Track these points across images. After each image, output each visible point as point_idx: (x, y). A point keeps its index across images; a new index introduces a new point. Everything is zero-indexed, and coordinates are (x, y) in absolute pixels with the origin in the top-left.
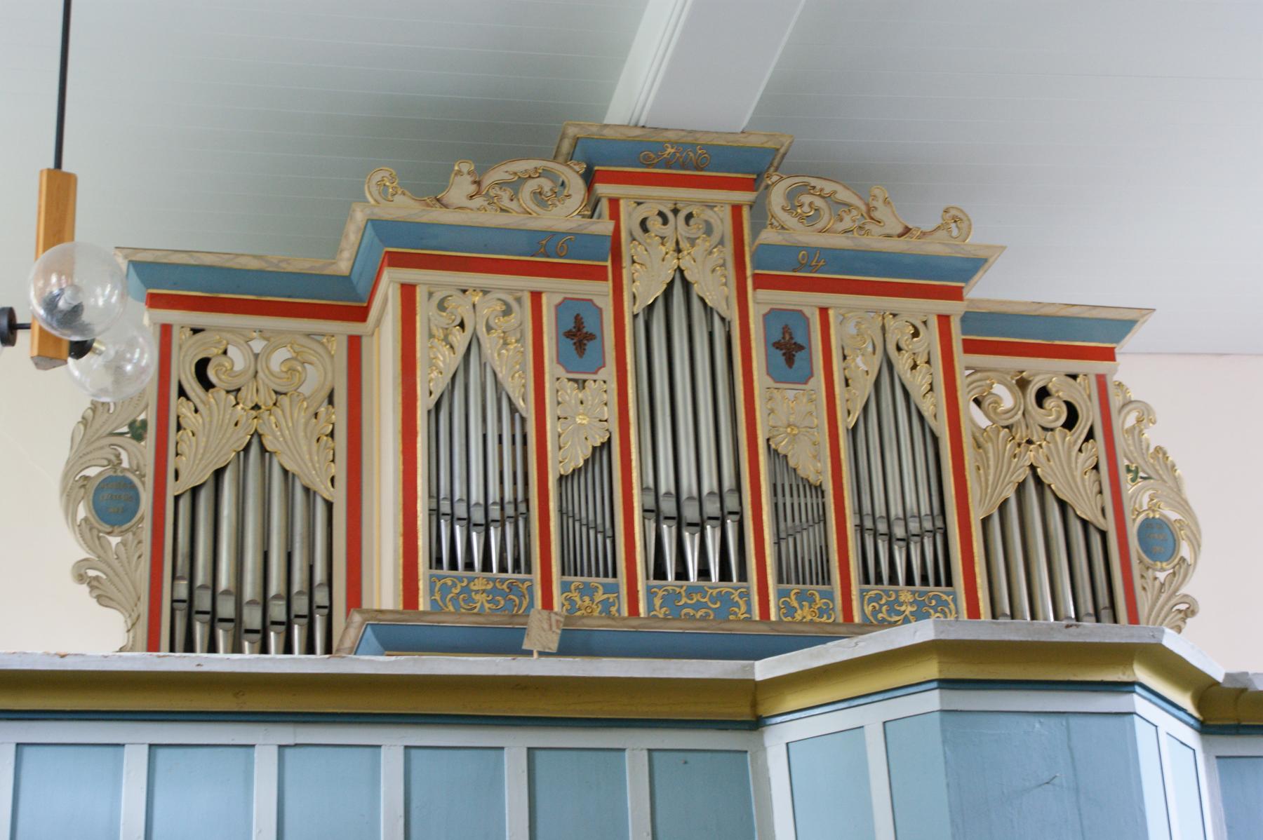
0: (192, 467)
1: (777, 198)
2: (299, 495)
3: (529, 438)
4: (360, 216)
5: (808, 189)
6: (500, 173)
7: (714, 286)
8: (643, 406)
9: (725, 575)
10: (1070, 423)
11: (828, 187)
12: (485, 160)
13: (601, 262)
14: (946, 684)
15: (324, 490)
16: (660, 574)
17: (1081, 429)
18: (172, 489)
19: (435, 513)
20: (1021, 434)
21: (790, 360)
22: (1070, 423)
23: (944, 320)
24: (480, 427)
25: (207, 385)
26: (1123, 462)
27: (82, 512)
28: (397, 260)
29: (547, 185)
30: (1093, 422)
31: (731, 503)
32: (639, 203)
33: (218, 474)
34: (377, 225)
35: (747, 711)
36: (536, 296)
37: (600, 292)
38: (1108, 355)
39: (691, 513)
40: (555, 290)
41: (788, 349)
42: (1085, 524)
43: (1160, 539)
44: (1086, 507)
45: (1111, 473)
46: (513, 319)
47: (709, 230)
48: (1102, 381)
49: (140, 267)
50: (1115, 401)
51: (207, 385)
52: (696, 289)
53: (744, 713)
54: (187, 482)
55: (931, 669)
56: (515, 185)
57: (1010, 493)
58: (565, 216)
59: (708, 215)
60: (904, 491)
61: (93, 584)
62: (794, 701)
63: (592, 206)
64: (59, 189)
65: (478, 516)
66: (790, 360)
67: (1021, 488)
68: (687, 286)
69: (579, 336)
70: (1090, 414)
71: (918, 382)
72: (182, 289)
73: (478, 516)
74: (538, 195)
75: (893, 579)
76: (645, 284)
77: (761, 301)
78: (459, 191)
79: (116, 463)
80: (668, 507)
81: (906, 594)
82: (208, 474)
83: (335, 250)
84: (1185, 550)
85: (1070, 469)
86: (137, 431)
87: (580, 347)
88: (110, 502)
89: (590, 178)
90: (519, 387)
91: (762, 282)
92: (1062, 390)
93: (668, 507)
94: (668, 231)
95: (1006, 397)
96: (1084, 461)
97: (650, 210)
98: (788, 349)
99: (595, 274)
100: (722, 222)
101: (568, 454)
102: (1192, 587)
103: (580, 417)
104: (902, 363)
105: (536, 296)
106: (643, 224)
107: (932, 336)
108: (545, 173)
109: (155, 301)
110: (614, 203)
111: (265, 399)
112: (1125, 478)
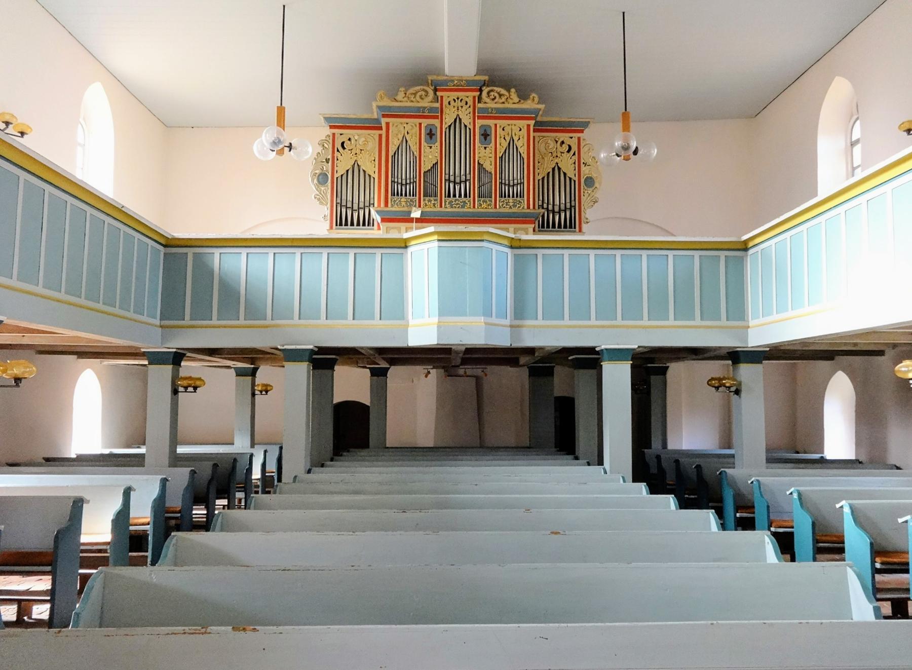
0: (341, 171)
1: (484, 94)
2: (367, 176)
3: (418, 160)
4: (374, 105)
5: (492, 91)
6: (412, 90)
7: (467, 120)
8: (446, 152)
9: (465, 196)
10: (569, 151)
11: (499, 89)
12: (408, 86)
13: (438, 113)
14: (439, 240)
15: (372, 175)
16: (449, 196)
17: (572, 152)
18: (336, 176)
19: (393, 182)
20: (554, 155)
21: (485, 139)
22: (569, 151)
23: (529, 126)
24: (403, 160)
25: (344, 148)
26: (582, 161)
27: (315, 181)
28: (384, 116)
29: (423, 93)
30: (575, 151)
31: (468, 178)
32: (448, 96)
33: (347, 171)
34: (379, 107)
35: (404, 245)
36: (420, 124)
37: (437, 122)
38: (582, 131)
39: (458, 180)
40: (425, 122)
41: (485, 135)
42: (570, 179)
43: (590, 182)
44: (570, 174)
45: (579, 164)
46: (414, 131)
47: (467, 103)
48: (579, 139)
49: (327, 119)
50: (582, 145)
51: (344, 148)
52: (463, 121)
53: (403, 245)
54: (339, 174)
55: (436, 237)
56: (415, 94)
57: (551, 170)
58: (426, 103)
59: (467, 100)
60: (514, 172)
61: (319, 200)
62: (413, 243)
63: (436, 99)
64: (281, 111)
65: (404, 182)
66: (485, 139)
67: (553, 169)
68: (460, 120)
69: (431, 135)
70: (575, 148)
71: (519, 144)
72: (337, 124)
73: (404, 182)
74: (421, 97)
75: (509, 196)
76: (449, 119)
77: (479, 123)
78: (400, 96)
79: (322, 169)
80: (452, 178)
81: (511, 200)
82: (345, 171)
83: (372, 113)
84: (597, 185)
85: (567, 164)
86: (327, 161)
87: (431, 138)
88: (322, 179)
89: (435, 90)
90: (415, 148)
91: (479, 118)
92: (568, 141)
93: (452, 178)
94: (456, 104)
95: (552, 144)
96: (572, 161)
97: (451, 99)
98: (485, 135)
99: (436, 117)
100: (470, 103)
101: (426, 166)
102: (598, 194)
103: (431, 155)
104: (516, 138)
105: (420, 124)
106: (343, 144)
107: (524, 131)
108: (424, 90)
109: (331, 127)
110: (442, 97)
111: (358, 151)
112: (582, 166)
